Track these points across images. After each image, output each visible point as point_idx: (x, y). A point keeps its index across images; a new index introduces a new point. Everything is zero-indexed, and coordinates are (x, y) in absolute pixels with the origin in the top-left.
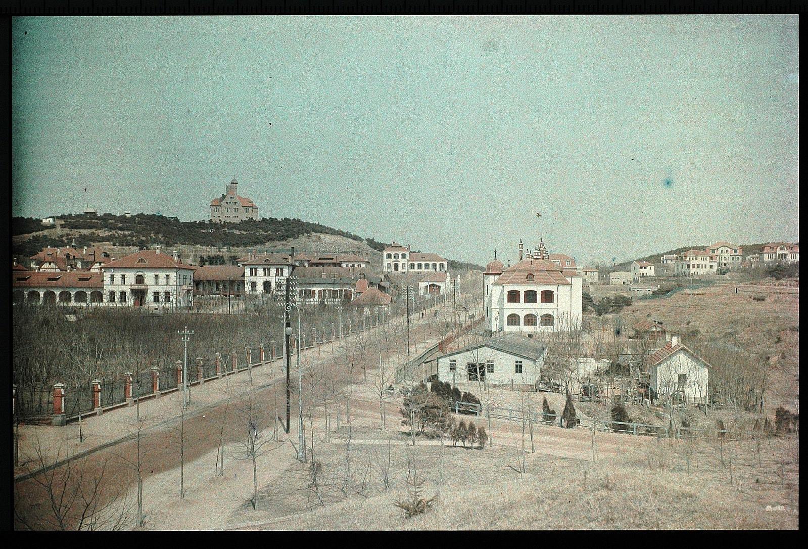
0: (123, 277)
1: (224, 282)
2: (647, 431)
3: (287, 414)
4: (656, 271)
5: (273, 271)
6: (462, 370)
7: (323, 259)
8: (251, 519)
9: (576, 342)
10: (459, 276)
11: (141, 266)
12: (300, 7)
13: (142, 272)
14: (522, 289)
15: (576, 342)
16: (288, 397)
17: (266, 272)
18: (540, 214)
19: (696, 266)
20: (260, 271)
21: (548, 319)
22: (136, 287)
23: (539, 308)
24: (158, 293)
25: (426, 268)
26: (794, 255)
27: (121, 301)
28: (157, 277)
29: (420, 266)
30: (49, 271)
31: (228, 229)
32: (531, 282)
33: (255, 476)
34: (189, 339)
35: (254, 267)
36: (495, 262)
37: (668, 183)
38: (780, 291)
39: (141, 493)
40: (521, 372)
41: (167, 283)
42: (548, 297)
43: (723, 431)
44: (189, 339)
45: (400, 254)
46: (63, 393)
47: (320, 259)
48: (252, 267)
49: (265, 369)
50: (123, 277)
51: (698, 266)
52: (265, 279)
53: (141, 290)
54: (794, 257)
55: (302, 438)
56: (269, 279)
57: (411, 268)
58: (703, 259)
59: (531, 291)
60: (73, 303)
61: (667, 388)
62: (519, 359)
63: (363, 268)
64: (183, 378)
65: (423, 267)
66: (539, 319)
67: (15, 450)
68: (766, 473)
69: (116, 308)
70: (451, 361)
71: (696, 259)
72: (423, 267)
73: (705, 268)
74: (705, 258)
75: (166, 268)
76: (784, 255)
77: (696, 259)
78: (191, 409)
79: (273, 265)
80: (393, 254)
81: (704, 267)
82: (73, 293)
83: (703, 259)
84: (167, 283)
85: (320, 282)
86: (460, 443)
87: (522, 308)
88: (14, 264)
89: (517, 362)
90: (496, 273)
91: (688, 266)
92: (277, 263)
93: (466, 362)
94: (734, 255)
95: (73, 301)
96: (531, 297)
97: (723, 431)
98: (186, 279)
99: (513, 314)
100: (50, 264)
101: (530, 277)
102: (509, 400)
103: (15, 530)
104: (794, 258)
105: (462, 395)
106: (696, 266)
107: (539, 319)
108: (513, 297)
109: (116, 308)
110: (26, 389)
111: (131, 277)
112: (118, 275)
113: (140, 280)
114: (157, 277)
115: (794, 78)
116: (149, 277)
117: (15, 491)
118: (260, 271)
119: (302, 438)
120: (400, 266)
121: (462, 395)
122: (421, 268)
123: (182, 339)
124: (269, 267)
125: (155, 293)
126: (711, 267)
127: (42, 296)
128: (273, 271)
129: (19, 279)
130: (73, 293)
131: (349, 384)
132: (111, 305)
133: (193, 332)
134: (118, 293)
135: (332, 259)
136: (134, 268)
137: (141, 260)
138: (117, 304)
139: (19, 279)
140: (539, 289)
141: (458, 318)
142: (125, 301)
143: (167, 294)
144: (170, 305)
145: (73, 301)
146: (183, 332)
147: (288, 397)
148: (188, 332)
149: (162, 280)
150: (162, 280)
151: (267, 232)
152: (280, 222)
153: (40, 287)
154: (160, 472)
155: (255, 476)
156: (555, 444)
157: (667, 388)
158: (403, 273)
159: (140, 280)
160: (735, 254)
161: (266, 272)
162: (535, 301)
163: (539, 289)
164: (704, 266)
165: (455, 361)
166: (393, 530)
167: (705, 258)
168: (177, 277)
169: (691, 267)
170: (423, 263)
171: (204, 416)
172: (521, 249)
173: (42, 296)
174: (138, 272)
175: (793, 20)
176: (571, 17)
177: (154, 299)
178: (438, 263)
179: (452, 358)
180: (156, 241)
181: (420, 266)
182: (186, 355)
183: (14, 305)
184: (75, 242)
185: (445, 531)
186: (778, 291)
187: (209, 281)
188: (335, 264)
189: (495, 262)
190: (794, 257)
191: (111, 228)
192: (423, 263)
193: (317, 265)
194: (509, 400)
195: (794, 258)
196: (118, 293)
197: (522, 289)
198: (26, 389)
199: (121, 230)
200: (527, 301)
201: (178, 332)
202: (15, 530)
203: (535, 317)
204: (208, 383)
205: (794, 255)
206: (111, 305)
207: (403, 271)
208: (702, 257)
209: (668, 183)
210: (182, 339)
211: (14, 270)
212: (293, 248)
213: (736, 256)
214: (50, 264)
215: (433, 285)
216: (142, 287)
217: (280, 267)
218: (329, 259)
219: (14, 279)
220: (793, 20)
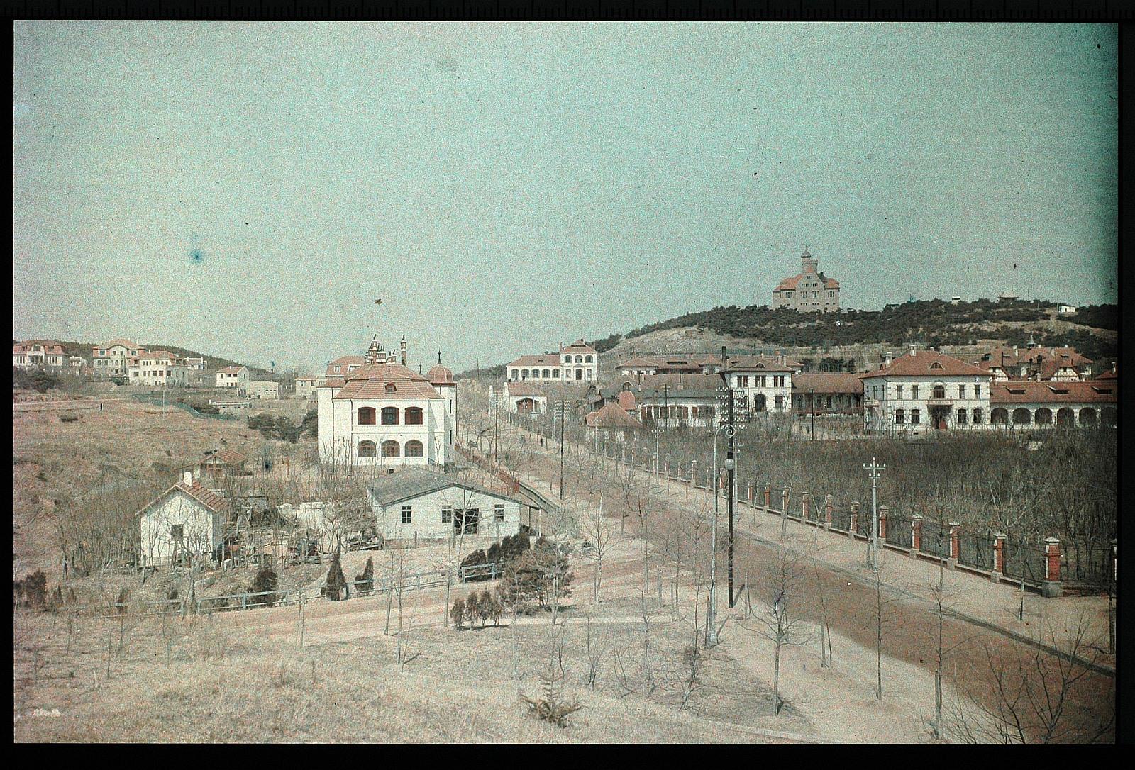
0: (915, 388)
1: (820, 396)
2: (227, 604)
3: (732, 580)
4: (215, 380)
5: (770, 381)
6: (487, 518)
7: (673, 363)
8: (783, 728)
9: (326, 479)
10: (491, 387)
11: (938, 373)
12: (714, 10)
13: (942, 381)
14: (378, 406)
15: (326, 479)
16: (730, 557)
17: (761, 381)
18: (377, 300)
19: (158, 374)
20: (752, 380)
21: (415, 448)
22: (935, 403)
23: (402, 432)
24: (918, 411)
25: (544, 377)
26: (21, 358)
27: (960, 422)
28: (962, 388)
29: (546, 373)
30: (1066, 380)
31: (760, 325)
32: (390, 396)
33: (777, 668)
34: (879, 475)
35: (779, 374)
36: (440, 368)
37: (197, 257)
38: (40, 408)
39: (937, 692)
40: (410, 521)
41: (900, 398)
42: (414, 416)
43: (120, 604)
44: (879, 475)
45: (584, 356)
46: (1047, 551)
47: (668, 363)
48: (758, 374)
49: (762, 517)
50: (915, 388)
51: (155, 374)
52: (757, 391)
53: (942, 406)
54: (21, 361)
55: (711, 614)
56: (763, 391)
57: (534, 376)
58: (149, 363)
59: (390, 408)
60: (1033, 426)
61: (198, 545)
62: (500, 502)
63: (625, 375)
64: (879, 531)
65: (541, 374)
66: (379, 448)
67: (1113, 631)
68: (59, 663)
69: (972, 432)
70: (404, 508)
71: (157, 363)
72: (541, 374)
73: (145, 372)
74: (149, 361)
75: (947, 375)
76: (35, 358)
77: (157, 363)
78: (866, 574)
79: (752, 372)
80: (573, 356)
81: (147, 373)
82: (1033, 411)
83: (149, 363)
84: (900, 398)
85: (686, 396)
86: (490, 622)
87: (378, 432)
88: (1115, 370)
89: (496, 506)
90: (438, 382)
91: (169, 373)
92: (746, 369)
93: (481, 508)
94: (101, 358)
95: (1033, 423)
96: (390, 416)
97: (120, 604)
98: (874, 391)
99: (415, 441)
100: (1065, 371)
101: (391, 388)
102: (421, 561)
103: (1114, 743)
104: (21, 362)
105: (486, 554)
106: (158, 374)
107: (379, 448)
108: (366, 416)
109: (972, 432)
110: (1098, 545)
111: (926, 388)
112: (908, 385)
113: (939, 392)
114: (962, 388)
115: (20, 110)
116: (951, 388)
117: (1114, 689)
118: (752, 380)
119: (711, 614)
120: (573, 374)
121: (486, 554)
122: (537, 376)
123: (870, 475)
124: (781, 374)
125: (913, 411)
126: (137, 374)
127: (1077, 415)
128: (770, 381)
129: (1108, 391)
130: (1033, 411)
131: (645, 539)
132: (979, 428)
133: (885, 465)
134: (970, 410)
135: (686, 363)
136: (903, 376)
137: (937, 365)
138: (970, 426)
139: (1108, 391)
140: (402, 405)
141: (492, 445)
142: (965, 422)
143: (915, 412)
144: (896, 428)
145: (1033, 423)
146: (871, 465)
147: (730, 557)
148: (878, 465)
149: (907, 393)
150: (907, 393)
151: (815, 321)
152: (742, 311)
153: (1073, 403)
154: (910, 663)
155: (777, 668)
156: (356, 623)
157: (198, 545)
158: (569, 383)
159: (939, 392)
160: (103, 356)
161: (761, 381)
162: (396, 422)
163: (402, 405)
164: (147, 375)
165: (410, 508)
166: (587, 744)
167: (149, 361)
168: (887, 388)
169: (165, 374)
170: (541, 369)
171: (849, 584)
172: (404, 350)
173: (1077, 415)
174: (936, 381)
175: (21, 27)
176: (367, 23)
177: (919, 419)
178: (520, 369)
179: (406, 504)
180: (916, 338)
181: (546, 373)
182: (875, 498)
183: (1116, 427)
184: (1034, 339)
185: (511, 745)
186: (37, 409)
187: (842, 395)
188: (690, 371)
189: (440, 368)
190: (21, 361)
191: (980, 320)
192: (541, 369)
193: (665, 371)
194: (421, 561)
195: (21, 362)
196: (970, 410)
197: (378, 406)
198: (1098, 545)
199: (965, 323)
200: (385, 422)
201: (864, 465)
202: (1114, 743)
203: (375, 444)
204: (843, 536)
205: (21, 358)
206: (979, 428)
207: (569, 380)
208: (145, 361)
209: (197, 257)
210: (870, 475)
211: (1115, 379)
212: (724, 348)
213: (104, 358)
214: (1065, 371)
215: (527, 400)
216: (944, 403)
217: (762, 374)
218: (682, 363)
219: (1115, 391)
220: (21, 27)
